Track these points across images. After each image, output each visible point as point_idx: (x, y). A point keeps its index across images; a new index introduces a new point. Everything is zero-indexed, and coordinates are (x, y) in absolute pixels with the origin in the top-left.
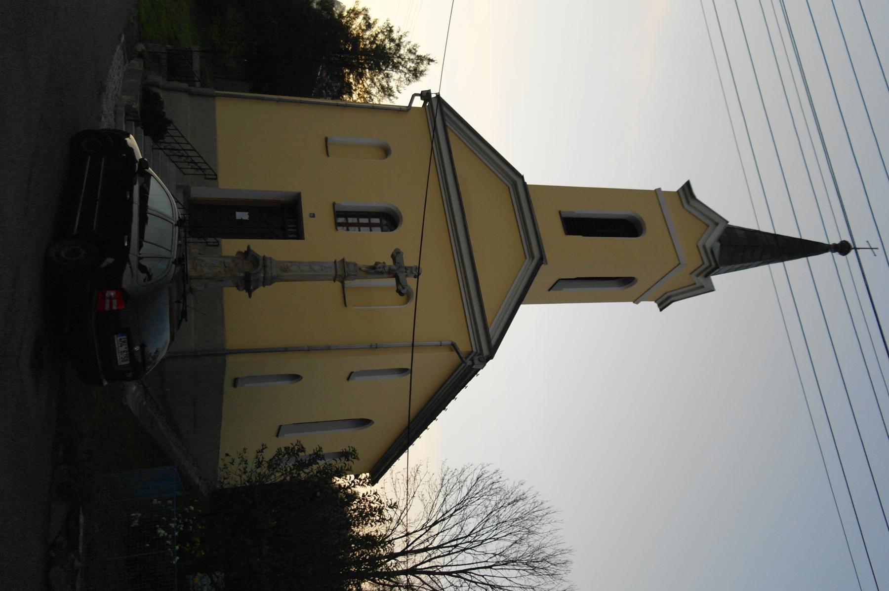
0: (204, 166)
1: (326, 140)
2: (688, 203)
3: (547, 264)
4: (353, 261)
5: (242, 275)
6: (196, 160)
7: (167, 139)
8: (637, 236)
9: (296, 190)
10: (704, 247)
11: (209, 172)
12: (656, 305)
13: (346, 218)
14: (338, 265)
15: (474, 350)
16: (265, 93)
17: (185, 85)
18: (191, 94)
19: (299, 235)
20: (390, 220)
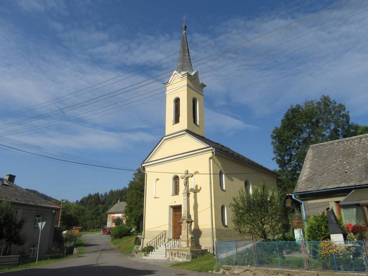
0: (162, 234)
1: (155, 198)
2: (170, 83)
3: (112, 191)
4: (183, 191)
5: (187, 223)
6: (160, 237)
7: (153, 245)
8: (179, 99)
9: (168, 207)
10: (182, 78)
11: (164, 233)
12: (204, 88)
13: (176, 191)
14: (184, 195)
15: (211, 151)
16: (53, 238)
17: (142, 240)
18: (144, 238)
19: (181, 205)
20: (176, 178)
